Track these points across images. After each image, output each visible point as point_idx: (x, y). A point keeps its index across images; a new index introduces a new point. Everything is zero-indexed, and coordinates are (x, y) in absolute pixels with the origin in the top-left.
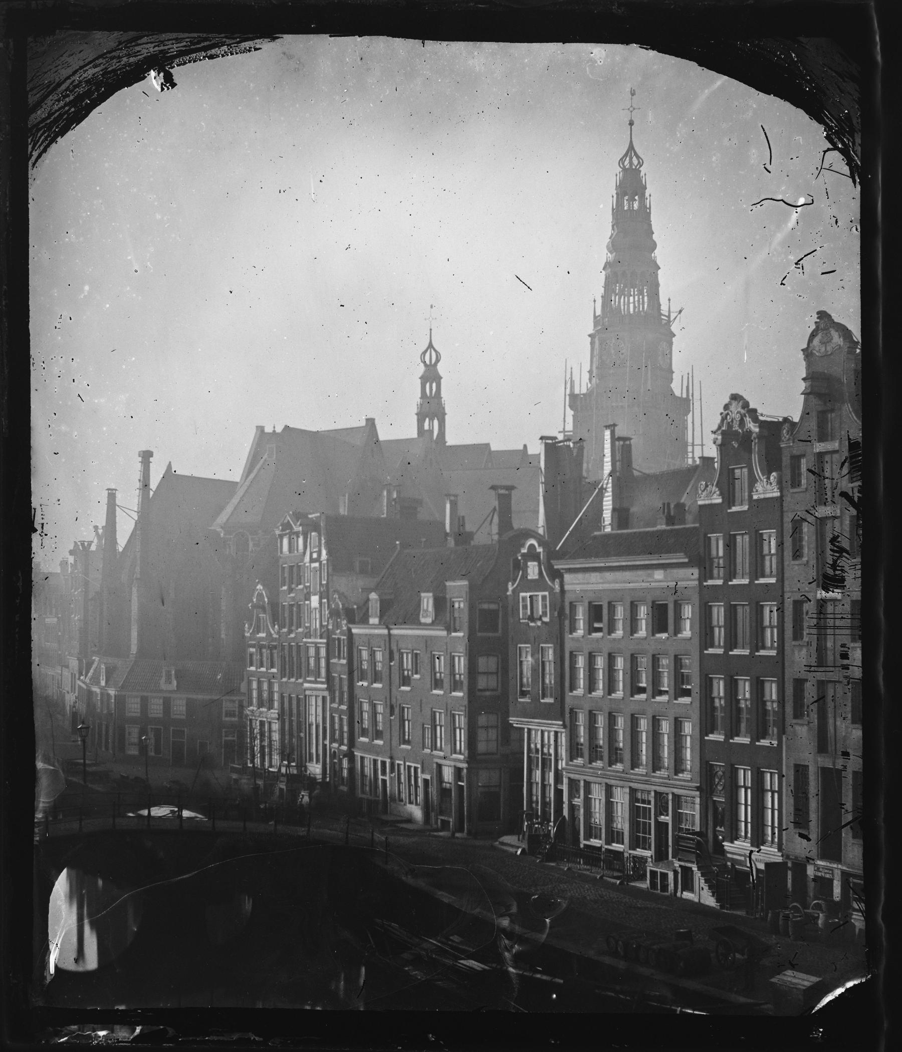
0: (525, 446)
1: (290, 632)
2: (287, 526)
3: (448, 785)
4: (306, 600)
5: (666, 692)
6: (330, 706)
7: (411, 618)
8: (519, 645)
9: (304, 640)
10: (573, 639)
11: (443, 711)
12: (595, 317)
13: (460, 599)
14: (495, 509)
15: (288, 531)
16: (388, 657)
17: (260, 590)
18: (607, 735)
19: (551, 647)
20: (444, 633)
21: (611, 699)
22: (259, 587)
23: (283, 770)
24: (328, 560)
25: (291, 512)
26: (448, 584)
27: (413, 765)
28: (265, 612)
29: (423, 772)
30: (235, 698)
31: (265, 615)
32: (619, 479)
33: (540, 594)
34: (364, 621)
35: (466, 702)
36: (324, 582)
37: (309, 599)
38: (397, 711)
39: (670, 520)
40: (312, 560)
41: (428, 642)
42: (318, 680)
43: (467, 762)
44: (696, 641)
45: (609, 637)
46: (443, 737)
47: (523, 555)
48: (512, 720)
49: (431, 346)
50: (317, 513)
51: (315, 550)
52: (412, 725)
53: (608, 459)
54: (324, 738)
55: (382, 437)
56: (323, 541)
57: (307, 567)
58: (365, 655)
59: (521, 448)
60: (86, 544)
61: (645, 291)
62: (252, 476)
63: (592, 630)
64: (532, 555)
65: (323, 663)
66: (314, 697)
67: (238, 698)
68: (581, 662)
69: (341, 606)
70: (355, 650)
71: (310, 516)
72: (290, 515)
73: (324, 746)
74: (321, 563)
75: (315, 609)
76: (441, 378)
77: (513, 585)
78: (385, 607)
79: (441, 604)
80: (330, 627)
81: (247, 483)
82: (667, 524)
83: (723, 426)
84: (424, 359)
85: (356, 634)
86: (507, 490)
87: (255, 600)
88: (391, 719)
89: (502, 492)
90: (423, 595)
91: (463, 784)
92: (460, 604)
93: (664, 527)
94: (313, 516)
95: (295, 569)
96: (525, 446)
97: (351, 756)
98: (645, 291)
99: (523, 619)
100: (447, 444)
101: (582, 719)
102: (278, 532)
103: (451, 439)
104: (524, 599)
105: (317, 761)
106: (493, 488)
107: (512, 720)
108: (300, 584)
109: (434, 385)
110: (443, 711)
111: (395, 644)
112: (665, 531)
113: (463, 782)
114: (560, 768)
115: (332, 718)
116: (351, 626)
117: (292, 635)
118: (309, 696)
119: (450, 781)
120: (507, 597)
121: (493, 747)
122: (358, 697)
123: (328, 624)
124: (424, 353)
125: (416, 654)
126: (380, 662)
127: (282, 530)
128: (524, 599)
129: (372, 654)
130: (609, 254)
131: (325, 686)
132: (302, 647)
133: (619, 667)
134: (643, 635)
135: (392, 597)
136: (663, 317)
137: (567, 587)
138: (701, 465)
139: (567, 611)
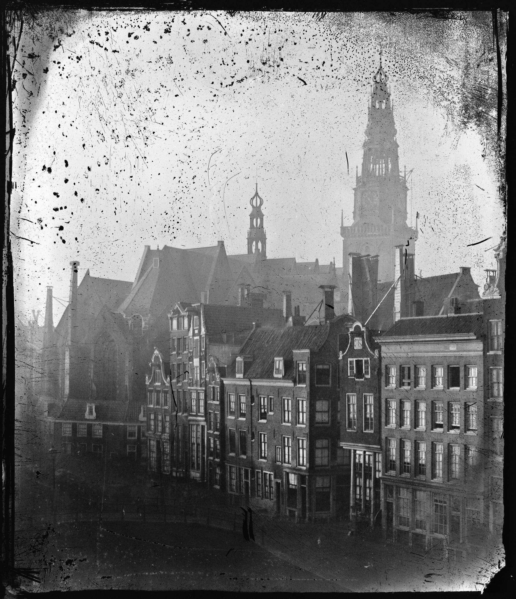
0: (317, 260)
1: (178, 382)
2: (177, 312)
3: (294, 487)
4: (189, 361)
5: (458, 428)
6: (207, 433)
7: (268, 374)
8: (347, 394)
9: (189, 388)
10: (387, 390)
11: (290, 437)
12: (357, 177)
13: (303, 362)
14: (322, 301)
15: (177, 315)
16: (250, 400)
17: (157, 354)
18: (399, 453)
19: (372, 395)
20: (291, 385)
21: (416, 432)
22: (156, 352)
23: (174, 474)
24: (206, 335)
25: (179, 303)
26: (294, 351)
27: (269, 473)
28: (160, 369)
29: (275, 478)
30: (135, 424)
31: (160, 371)
32: (405, 281)
33: (364, 359)
34: (233, 375)
35: (307, 431)
36: (203, 349)
37: (192, 361)
38: (256, 437)
39: (458, 310)
40: (194, 335)
41: (279, 391)
42: (198, 414)
43: (309, 472)
44: (481, 393)
45: (415, 389)
46: (290, 454)
47: (352, 333)
48: (342, 444)
49: (257, 194)
50: (198, 303)
51: (196, 328)
52: (268, 446)
53: (398, 268)
54: (203, 453)
55: (227, 254)
56: (202, 322)
57: (191, 339)
58: (233, 398)
59: (314, 261)
60: (31, 322)
61: (389, 161)
62: (143, 278)
63: (401, 384)
64: (358, 333)
65: (202, 403)
66: (196, 426)
67: (138, 424)
68: (394, 405)
69: (215, 366)
70: (226, 395)
71: (193, 305)
72: (178, 304)
73: (203, 458)
74: (200, 336)
75: (197, 367)
76: (264, 215)
77: (343, 353)
78: (247, 366)
79: (289, 365)
80: (208, 379)
81: (140, 283)
82: (455, 313)
83: (502, 245)
84: (252, 202)
85: (228, 385)
86: (330, 288)
87: (153, 361)
88: (252, 442)
89: (327, 290)
90: (275, 359)
91: (305, 486)
92: (304, 367)
93: (453, 315)
94: (195, 305)
95: (181, 341)
96: (317, 260)
97: (222, 466)
98: (389, 161)
99: (350, 376)
100: (267, 258)
101: (394, 445)
102: (169, 316)
103: (270, 255)
104: (351, 362)
105: (198, 469)
106: (322, 287)
107: (342, 444)
108: (185, 350)
109: (259, 220)
110: (290, 437)
111: (256, 392)
112: (454, 317)
113: (305, 484)
114: (377, 477)
115: (209, 440)
116: (222, 379)
117: (180, 384)
118: (192, 425)
119: (296, 484)
120: (339, 361)
121: (325, 461)
122: (227, 426)
123: (206, 377)
124: (252, 199)
125: (271, 398)
126: (244, 403)
127: (173, 315)
128: (351, 362)
129: (238, 398)
130: (366, 137)
131: (204, 419)
132: (186, 393)
133: (407, 409)
134: (441, 388)
135: (252, 360)
136: (400, 178)
137: (383, 355)
138: (461, 272)
139: (383, 371)
